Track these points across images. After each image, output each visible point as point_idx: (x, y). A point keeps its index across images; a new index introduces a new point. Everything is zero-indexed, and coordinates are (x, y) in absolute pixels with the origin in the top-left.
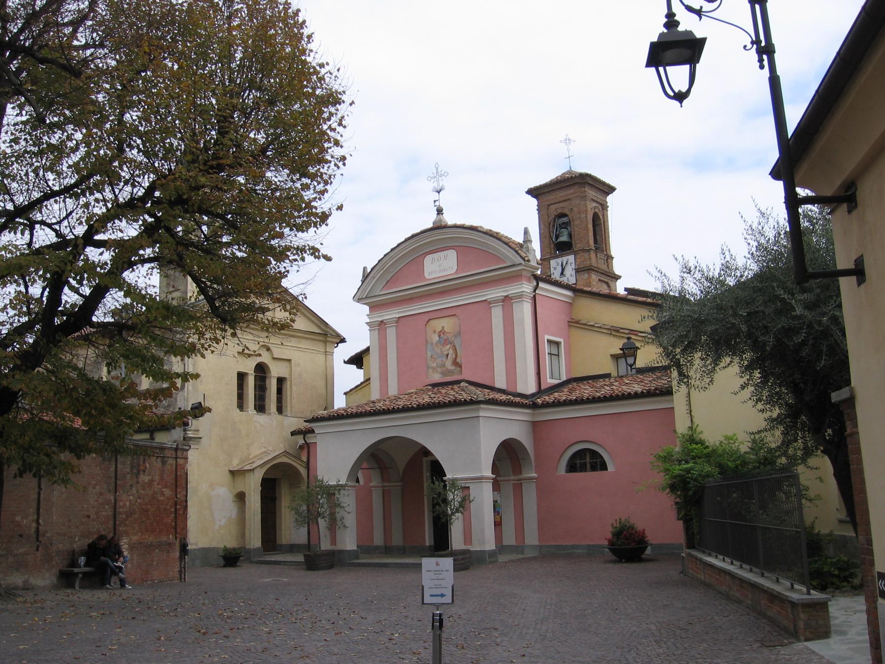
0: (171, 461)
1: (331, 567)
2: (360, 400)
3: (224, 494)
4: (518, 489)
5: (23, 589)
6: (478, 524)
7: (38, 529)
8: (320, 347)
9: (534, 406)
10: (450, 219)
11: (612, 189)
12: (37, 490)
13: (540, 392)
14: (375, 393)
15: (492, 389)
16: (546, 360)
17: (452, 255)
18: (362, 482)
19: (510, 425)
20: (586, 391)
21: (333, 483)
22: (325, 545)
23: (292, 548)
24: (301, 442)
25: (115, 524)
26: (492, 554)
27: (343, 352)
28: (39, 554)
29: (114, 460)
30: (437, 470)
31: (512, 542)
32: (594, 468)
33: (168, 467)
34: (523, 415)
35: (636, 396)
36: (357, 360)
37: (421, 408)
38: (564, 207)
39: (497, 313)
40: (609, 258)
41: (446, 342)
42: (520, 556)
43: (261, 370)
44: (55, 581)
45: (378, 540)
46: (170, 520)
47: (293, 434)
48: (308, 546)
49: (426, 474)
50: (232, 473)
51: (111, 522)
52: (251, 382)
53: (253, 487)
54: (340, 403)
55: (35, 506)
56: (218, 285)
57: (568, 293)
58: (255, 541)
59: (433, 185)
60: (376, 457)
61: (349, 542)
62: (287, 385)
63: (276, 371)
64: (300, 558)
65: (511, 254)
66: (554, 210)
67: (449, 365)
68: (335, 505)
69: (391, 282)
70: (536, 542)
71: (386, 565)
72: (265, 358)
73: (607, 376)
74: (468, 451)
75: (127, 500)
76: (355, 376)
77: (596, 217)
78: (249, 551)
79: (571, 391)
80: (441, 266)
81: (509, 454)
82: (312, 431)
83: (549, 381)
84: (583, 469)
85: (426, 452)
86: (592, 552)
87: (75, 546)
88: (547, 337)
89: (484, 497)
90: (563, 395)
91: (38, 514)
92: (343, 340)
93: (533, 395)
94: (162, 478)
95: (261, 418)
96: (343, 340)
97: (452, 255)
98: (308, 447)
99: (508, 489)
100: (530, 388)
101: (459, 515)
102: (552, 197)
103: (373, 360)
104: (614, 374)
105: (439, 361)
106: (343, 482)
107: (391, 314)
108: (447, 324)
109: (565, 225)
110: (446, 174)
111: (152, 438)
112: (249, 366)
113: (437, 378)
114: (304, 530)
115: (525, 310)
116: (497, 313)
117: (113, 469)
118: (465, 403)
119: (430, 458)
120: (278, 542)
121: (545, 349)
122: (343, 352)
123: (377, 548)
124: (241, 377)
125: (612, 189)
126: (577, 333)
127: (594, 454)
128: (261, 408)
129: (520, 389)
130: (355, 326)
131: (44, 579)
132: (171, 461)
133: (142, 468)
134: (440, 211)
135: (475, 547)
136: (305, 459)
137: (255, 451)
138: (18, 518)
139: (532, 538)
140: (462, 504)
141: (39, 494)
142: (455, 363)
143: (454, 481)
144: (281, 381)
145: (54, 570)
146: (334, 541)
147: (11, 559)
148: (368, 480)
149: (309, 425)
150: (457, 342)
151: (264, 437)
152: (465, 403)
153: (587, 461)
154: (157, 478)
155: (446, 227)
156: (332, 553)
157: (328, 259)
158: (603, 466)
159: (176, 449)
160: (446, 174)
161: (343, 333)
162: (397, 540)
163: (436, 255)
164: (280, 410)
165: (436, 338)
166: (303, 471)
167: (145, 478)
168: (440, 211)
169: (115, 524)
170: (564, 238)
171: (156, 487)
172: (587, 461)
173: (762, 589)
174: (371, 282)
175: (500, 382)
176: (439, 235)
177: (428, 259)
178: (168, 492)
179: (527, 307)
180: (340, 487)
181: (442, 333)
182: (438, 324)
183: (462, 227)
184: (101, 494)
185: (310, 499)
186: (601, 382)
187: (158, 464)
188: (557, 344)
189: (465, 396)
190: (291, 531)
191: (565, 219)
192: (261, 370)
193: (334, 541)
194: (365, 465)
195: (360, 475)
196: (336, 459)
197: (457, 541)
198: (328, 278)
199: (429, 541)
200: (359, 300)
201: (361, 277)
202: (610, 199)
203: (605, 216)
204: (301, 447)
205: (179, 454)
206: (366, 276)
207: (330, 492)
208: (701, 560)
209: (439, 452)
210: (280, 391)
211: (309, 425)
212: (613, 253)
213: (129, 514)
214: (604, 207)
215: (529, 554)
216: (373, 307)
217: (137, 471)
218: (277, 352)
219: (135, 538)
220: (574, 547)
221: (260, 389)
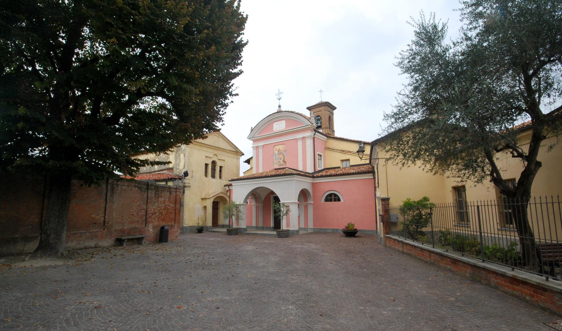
0: (174, 193)
1: (237, 234)
2: (248, 174)
3: (199, 206)
4: (306, 207)
5: (95, 248)
6: (292, 220)
7: (104, 221)
8: (235, 156)
9: (313, 177)
10: (283, 109)
11: (335, 108)
12: (105, 203)
13: (315, 172)
14: (254, 172)
15: (297, 171)
16: (317, 161)
17: (284, 122)
18: (249, 203)
19: (306, 184)
20: (333, 172)
21: (238, 203)
22: (235, 226)
23: (223, 226)
24: (228, 189)
25: (146, 218)
26: (297, 231)
27: (243, 158)
28: (105, 232)
29: (146, 193)
30: (277, 199)
31: (303, 227)
32: (335, 201)
33: (172, 195)
34: (310, 180)
35: (353, 174)
36: (248, 161)
37: (272, 176)
38: (319, 114)
39: (300, 143)
40: (334, 131)
41: (281, 154)
42: (306, 232)
43: (214, 163)
44: (113, 243)
45: (254, 224)
46: (172, 216)
47: (225, 186)
48: (229, 226)
49: (272, 200)
50: (202, 199)
51: (144, 217)
52: (210, 167)
53: (209, 204)
54: (242, 175)
55: (103, 209)
56: (135, 11)
57: (326, 138)
58: (209, 223)
59: (277, 97)
60: (254, 194)
61: (243, 225)
62: (223, 169)
63: (219, 164)
64: (225, 230)
65: (306, 121)
66: (317, 114)
67: (281, 162)
68: (238, 211)
69: (261, 132)
70: (312, 227)
71: (257, 234)
72: (215, 159)
73: (339, 167)
74: (287, 192)
75: (152, 208)
76: (248, 167)
77: (330, 117)
78: (207, 227)
79: (326, 172)
80: (280, 126)
81: (304, 194)
82: (231, 185)
83: (318, 169)
84: (331, 200)
85: (272, 193)
86: (334, 232)
87: (125, 228)
88: (318, 153)
89: (294, 211)
90: (324, 173)
91: (105, 214)
92: (243, 154)
93: (313, 173)
94: (169, 200)
95: (213, 180)
96: (243, 154)
97: (284, 122)
98: (230, 190)
99: (302, 207)
100: (310, 170)
101: (285, 216)
102: (315, 110)
103: (253, 162)
104: (341, 167)
105: (278, 161)
106: (242, 203)
107: (261, 144)
108: (281, 147)
109: (318, 120)
110: (282, 93)
111: (167, 184)
112: (209, 162)
113: (277, 166)
114: (228, 220)
115: (309, 143)
116: (300, 143)
117: (146, 195)
118: (289, 174)
119: (274, 195)
120: (219, 224)
121: (317, 157)
122: (243, 158)
123: (253, 227)
124: (206, 165)
125: (335, 108)
126: (328, 152)
127: (335, 195)
128: (213, 176)
129: (308, 171)
130: (247, 148)
131: (108, 242)
132: (174, 193)
133: (160, 195)
134: (280, 106)
135: (291, 229)
136: (228, 195)
137: (211, 192)
138: (94, 216)
139: (311, 225)
140: (287, 213)
141: (106, 205)
142: (284, 161)
143: (284, 204)
144: (221, 167)
145: (113, 238)
146: (238, 224)
147: (88, 234)
148: (251, 203)
149: (230, 182)
150: (285, 154)
151: (214, 187)
152: (289, 174)
153: (333, 198)
154: (167, 200)
155: (282, 112)
156: (237, 229)
157: (237, 95)
158: (339, 200)
159: (176, 188)
160: (282, 93)
161: (243, 152)
162: (261, 225)
163: (277, 123)
164: (220, 177)
165: (277, 152)
166: (228, 199)
167: (162, 199)
168: (280, 106)
169: (146, 218)
170: (319, 125)
171: (167, 203)
172: (333, 198)
173: (487, 270)
174: (254, 132)
175: (300, 169)
176: (280, 114)
177: (275, 124)
178: (172, 205)
179: (312, 141)
180: (240, 205)
181: (279, 150)
182: (278, 147)
183: (288, 112)
184: (140, 205)
185: (230, 210)
186: (337, 170)
187: (168, 194)
188: (321, 156)
189: (288, 172)
190: (223, 221)
191: (319, 118)
192: (214, 163)
193: (238, 224)
194: (250, 197)
195: (248, 201)
196: (239, 194)
197: (284, 226)
198: (238, 120)
199: (272, 225)
200: (249, 139)
201: (250, 131)
202: (335, 111)
203: (333, 117)
204: (228, 191)
205: (177, 190)
206: (252, 130)
207: (237, 207)
208: (392, 238)
209: (278, 194)
210: (220, 171)
211: (230, 182)
212: (335, 130)
213: (153, 214)
214: (333, 114)
215: (310, 231)
216: (254, 141)
217: (158, 196)
218: (220, 157)
219: (156, 224)
220: (327, 229)
221: (213, 169)
